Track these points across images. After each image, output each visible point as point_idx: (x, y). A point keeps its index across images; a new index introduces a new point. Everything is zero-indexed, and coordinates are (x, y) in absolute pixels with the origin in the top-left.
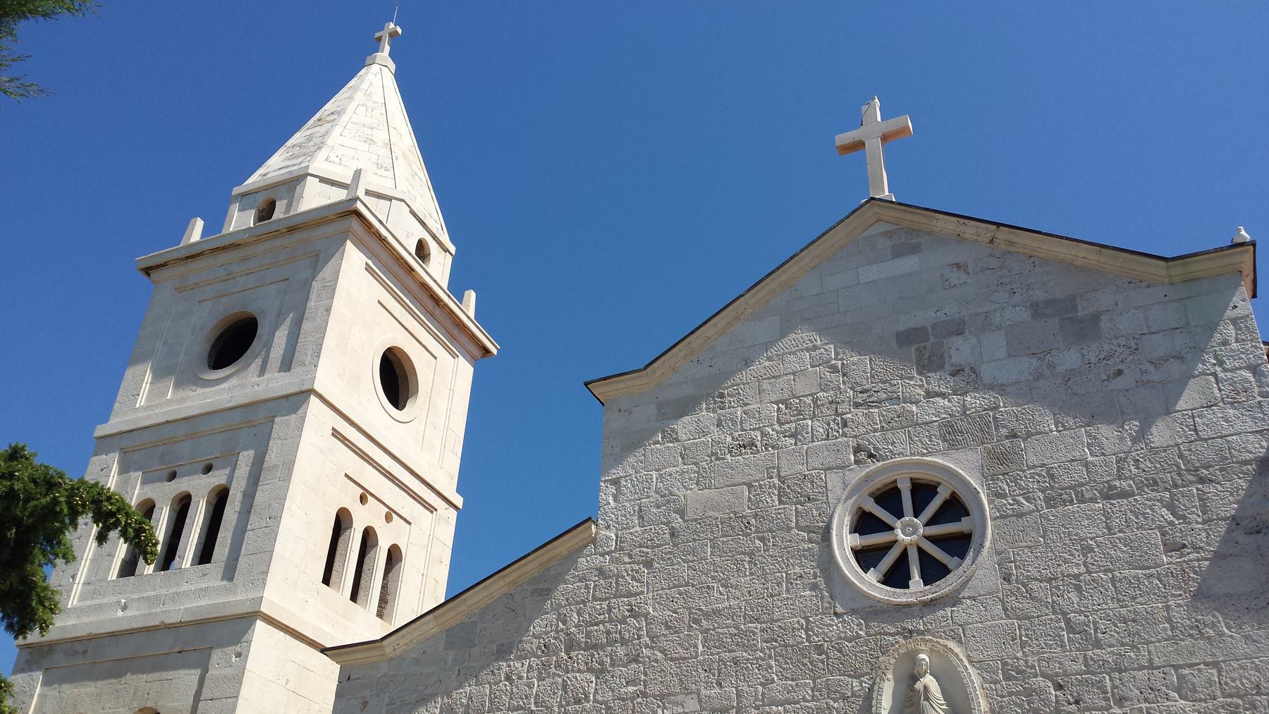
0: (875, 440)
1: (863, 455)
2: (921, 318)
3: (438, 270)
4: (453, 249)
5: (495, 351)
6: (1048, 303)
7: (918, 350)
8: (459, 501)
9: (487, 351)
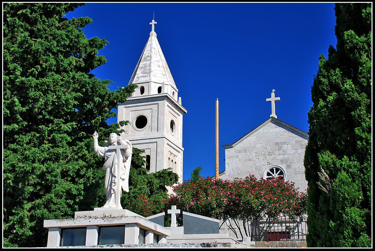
0: (270, 161)
1: (268, 164)
2: (279, 141)
3: (180, 104)
4: (178, 90)
5: (187, 112)
6: (298, 141)
7: (278, 146)
8: (183, 149)
9: (185, 112)
